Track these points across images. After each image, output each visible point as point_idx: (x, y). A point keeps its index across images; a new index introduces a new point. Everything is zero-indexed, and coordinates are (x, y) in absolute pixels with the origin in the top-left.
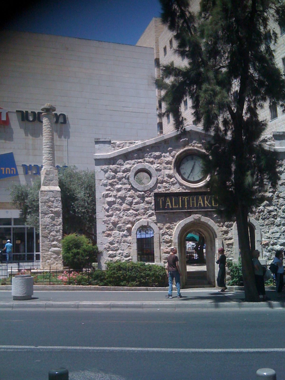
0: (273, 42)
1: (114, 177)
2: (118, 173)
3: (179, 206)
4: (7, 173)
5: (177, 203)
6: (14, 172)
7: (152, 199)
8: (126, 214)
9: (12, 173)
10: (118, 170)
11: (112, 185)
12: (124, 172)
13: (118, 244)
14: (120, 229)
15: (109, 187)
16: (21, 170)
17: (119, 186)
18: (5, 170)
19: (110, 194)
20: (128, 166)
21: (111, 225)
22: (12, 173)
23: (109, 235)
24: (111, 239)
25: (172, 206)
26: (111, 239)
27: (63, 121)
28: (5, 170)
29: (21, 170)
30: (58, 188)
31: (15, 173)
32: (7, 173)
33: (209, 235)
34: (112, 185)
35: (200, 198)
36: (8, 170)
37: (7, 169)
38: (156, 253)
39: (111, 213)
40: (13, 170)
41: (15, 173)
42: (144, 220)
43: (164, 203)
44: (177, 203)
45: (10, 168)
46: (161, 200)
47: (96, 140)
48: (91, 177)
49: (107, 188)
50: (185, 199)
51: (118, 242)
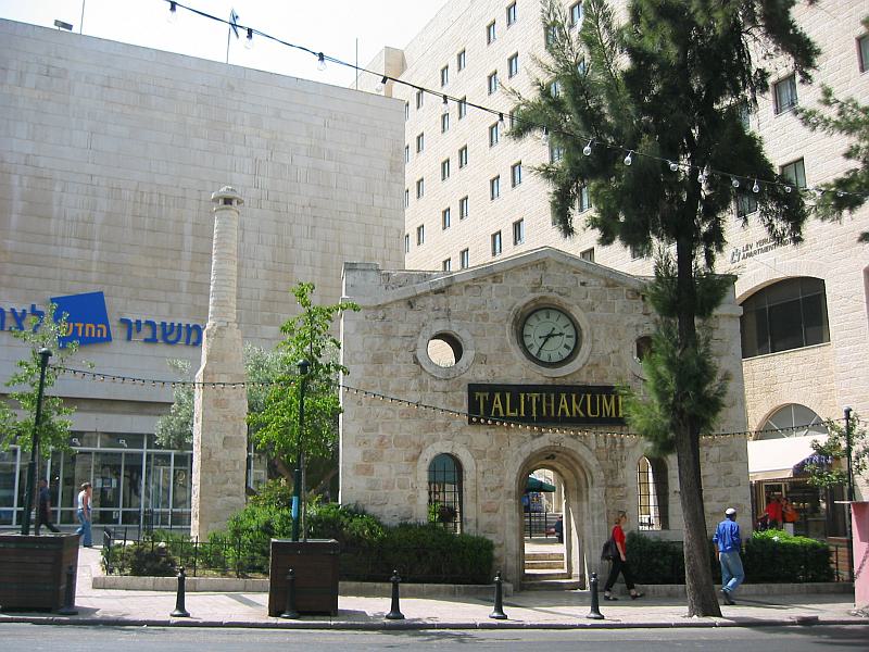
0: (577, 207)
3: (519, 413)
4: (87, 335)
5: (515, 405)
6: (102, 334)
9: (99, 335)
16: (118, 332)
18: (84, 328)
22: (99, 335)
25: (505, 412)
27: (149, 337)
28: (84, 328)
29: (118, 332)
31: (105, 336)
32: (87, 335)
33: (577, 477)
35: (563, 396)
36: (90, 329)
37: (88, 325)
38: (663, 619)
40: (101, 329)
41: (105, 336)
43: (489, 404)
44: (515, 405)
45: (96, 325)
46: (481, 396)
48: (708, 290)
50: (531, 398)
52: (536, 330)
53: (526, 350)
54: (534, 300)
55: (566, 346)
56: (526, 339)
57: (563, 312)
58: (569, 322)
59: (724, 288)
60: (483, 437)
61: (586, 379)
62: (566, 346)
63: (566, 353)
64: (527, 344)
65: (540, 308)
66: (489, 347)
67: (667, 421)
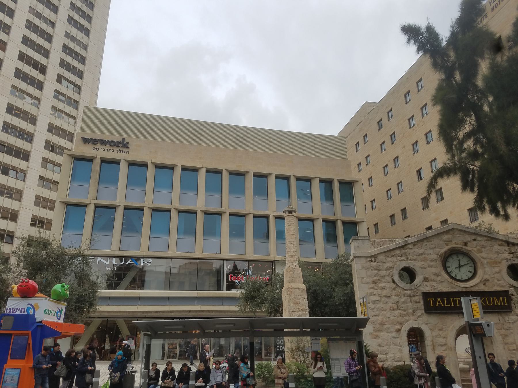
1: (376, 275)
2: (380, 271)
5: (449, 302)
7: (420, 298)
8: (393, 314)
10: (381, 268)
11: (374, 282)
12: (386, 270)
13: (387, 347)
14: (388, 331)
15: (372, 285)
17: (383, 285)
19: (375, 293)
20: (391, 264)
21: (378, 326)
23: (377, 337)
24: (379, 341)
26: (379, 341)
30: (303, 286)
34: (374, 282)
36: (490, 303)
39: (377, 313)
42: (413, 323)
44: (449, 302)
47: (126, 150)
49: (371, 286)
51: (387, 345)
52: (452, 264)
53: (449, 274)
54: (449, 250)
55: (470, 272)
56: (457, 278)
57: (466, 254)
58: (473, 272)
59: (395, 373)
60: (434, 320)
61: (482, 288)
62: (470, 272)
63: (470, 275)
64: (449, 271)
65: (453, 252)
66: (430, 272)
67: (91, 278)
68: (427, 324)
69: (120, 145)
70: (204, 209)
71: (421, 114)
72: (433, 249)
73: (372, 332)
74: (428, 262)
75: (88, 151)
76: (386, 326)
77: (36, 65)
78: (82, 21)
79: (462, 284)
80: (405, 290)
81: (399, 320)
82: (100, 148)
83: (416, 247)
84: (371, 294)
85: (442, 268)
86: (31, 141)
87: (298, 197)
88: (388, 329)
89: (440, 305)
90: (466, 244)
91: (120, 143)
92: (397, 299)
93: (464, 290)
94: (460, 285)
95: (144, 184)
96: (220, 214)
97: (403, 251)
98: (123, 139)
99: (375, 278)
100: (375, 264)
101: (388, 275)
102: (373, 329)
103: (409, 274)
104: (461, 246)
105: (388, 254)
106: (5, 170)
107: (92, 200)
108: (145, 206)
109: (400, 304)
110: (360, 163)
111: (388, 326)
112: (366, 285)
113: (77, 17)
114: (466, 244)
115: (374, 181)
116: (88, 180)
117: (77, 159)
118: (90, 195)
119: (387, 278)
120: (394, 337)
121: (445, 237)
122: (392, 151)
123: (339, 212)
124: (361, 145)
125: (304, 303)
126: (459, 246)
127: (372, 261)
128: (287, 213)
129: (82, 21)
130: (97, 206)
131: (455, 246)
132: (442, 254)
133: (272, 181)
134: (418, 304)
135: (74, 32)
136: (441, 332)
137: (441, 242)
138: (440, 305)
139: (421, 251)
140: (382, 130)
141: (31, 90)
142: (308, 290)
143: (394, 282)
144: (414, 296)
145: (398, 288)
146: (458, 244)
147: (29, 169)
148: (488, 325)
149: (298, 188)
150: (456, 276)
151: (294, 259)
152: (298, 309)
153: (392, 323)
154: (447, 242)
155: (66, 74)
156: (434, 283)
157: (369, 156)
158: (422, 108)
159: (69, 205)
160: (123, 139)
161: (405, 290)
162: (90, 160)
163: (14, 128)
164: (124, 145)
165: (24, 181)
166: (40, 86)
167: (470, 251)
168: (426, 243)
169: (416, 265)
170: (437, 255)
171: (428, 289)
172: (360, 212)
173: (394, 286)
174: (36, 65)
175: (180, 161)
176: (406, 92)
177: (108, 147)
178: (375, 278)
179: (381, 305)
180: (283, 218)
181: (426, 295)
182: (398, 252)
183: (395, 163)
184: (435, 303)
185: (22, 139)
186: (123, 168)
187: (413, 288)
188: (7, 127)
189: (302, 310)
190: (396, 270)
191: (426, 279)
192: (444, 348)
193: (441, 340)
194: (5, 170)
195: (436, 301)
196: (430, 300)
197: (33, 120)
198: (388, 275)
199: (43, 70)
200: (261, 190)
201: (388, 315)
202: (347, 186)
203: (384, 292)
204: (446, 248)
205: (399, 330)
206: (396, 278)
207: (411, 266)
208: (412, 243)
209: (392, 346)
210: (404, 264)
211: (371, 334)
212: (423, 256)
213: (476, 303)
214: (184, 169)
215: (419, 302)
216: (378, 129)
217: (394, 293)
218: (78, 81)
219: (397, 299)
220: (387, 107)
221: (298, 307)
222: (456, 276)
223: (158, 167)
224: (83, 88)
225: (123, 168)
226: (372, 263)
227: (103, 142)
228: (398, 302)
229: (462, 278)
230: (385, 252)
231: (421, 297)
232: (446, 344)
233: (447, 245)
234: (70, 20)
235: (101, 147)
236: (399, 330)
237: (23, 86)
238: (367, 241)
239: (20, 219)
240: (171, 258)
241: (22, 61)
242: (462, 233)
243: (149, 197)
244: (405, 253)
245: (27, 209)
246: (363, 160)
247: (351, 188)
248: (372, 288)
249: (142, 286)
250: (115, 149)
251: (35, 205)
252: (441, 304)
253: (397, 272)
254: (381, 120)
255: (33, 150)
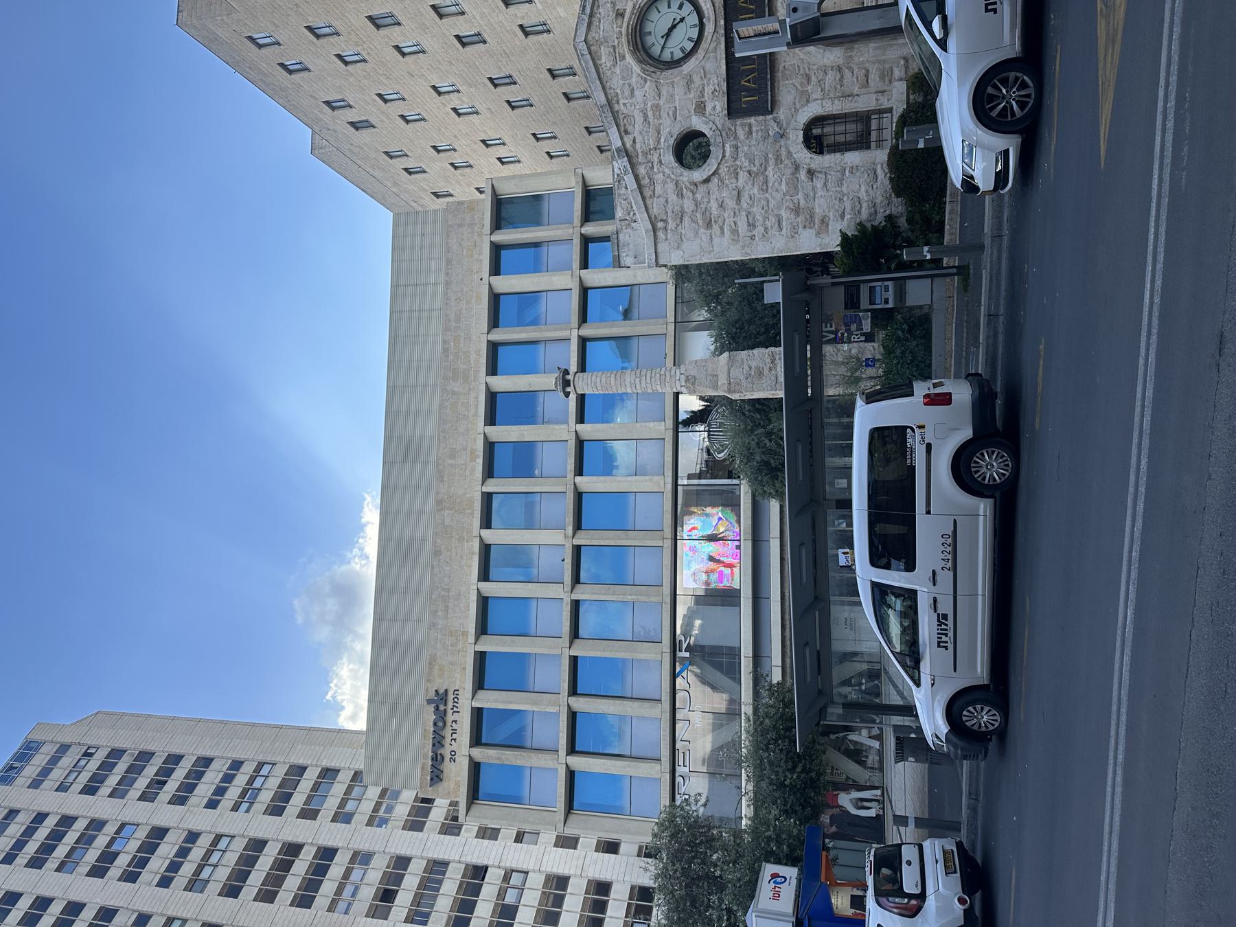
11: (709, 225)
12: (681, 195)
15: (716, 228)
17: (714, 205)
20: (671, 186)
21: (801, 219)
34: (709, 225)
39: (773, 219)
47: (451, 697)
49: (718, 232)
53: (688, 56)
60: (786, 94)
68: (796, 110)
69: (442, 707)
70: (570, 530)
71: (331, 39)
72: (632, 91)
73: (813, 231)
74: (661, 102)
75: (457, 773)
76: (802, 202)
77: (283, 866)
78: (180, 774)
79: (710, 28)
80: (724, 156)
81: (789, 172)
82: (452, 748)
83: (630, 128)
84: (735, 232)
85: (675, 71)
86: (445, 864)
87: (535, 322)
88: (807, 196)
89: (755, 81)
90: (620, 15)
91: (437, 708)
92: (743, 176)
93: (722, 22)
94: (712, 30)
95: (522, 659)
96: (579, 496)
97: (641, 158)
98: (429, 702)
99: (700, 222)
100: (670, 220)
101: (694, 194)
102: (808, 230)
103: (691, 148)
104: (625, 25)
105: (648, 193)
106: (506, 913)
107: (560, 762)
108: (567, 653)
109: (755, 169)
110: (452, 164)
111: (800, 196)
112: (716, 240)
113: (172, 786)
114: (620, 15)
115: (491, 135)
116: (516, 772)
117: (474, 794)
118: (546, 770)
119: (698, 196)
120: (825, 184)
121: (605, 60)
122: (421, 101)
123: (562, 230)
124: (410, 163)
125: (759, 356)
126: (624, 31)
127: (665, 228)
128: (568, 389)
129: (180, 774)
130: (572, 750)
131: (624, 39)
132: (644, 71)
133: (501, 383)
134: (754, 129)
135: (205, 789)
136: (813, 79)
137: (618, 70)
138: (755, 81)
139: (639, 119)
140: (373, 121)
141: (336, 870)
142: (730, 350)
143: (707, 181)
144: (736, 138)
145: (720, 171)
146: (621, 33)
147: (502, 864)
148: (795, 10)
149: (513, 224)
150: (690, 39)
151: (668, 378)
152: (770, 369)
153: (796, 187)
154: (618, 58)
155: (298, 800)
156: (708, 90)
157: (434, 147)
158: (318, 36)
159: (570, 807)
160: (429, 702)
161: (724, 156)
162: (475, 768)
163: (418, 900)
164: (440, 701)
165: (527, 873)
166: (327, 854)
167: (634, 6)
168: (622, 107)
169: (671, 130)
170: (645, 80)
171: (718, 105)
172: (559, 182)
173: (715, 180)
174: (283, 866)
175: (470, 585)
176: (283, 72)
177: (447, 733)
178: (700, 222)
179: (756, 210)
180: (581, 399)
181: (734, 111)
182: (642, 171)
183: (449, 92)
184: (750, 92)
185: (440, 882)
186: (489, 700)
187: (719, 140)
188: (418, 914)
189: (773, 361)
190: (681, 175)
191: (700, 108)
192: (847, 73)
193: (831, 77)
194: (506, 913)
195: (747, 90)
196: (745, 103)
197: (402, 862)
198: (694, 194)
199: (293, 850)
200: (521, 407)
201: (779, 196)
202: (504, 210)
203: (730, 203)
204: (629, 59)
205: (811, 173)
206: (698, 175)
207: (672, 141)
208: (622, 138)
209: (844, 189)
210: (669, 158)
211: (818, 234)
212: (650, 114)
213: (745, 28)
214: (484, 576)
215: (750, 126)
216: (371, 130)
217: (731, 183)
218: (311, 775)
219: (743, 176)
220: (321, 111)
221: (766, 371)
222: (690, 39)
223: (483, 629)
224: (326, 763)
225: (489, 700)
226: (669, 227)
227: (438, 742)
228: (750, 173)
229: (694, 26)
230: (644, 198)
231: (739, 122)
232: (839, 69)
233: (624, 57)
234: (179, 799)
235: (447, 745)
236: (811, 173)
237: (328, 887)
238: (621, 236)
239: (604, 876)
240: (676, 540)
241: (276, 893)
242: (595, 23)
243: (548, 652)
244: (645, 154)
245: (584, 865)
246: (443, 161)
247: (511, 201)
248: (722, 228)
249: (734, 653)
250: (450, 718)
251: (575, 848)
252: (750, 88)
253: (686, 173)
254: (352, 124)
255: (463, 859)
